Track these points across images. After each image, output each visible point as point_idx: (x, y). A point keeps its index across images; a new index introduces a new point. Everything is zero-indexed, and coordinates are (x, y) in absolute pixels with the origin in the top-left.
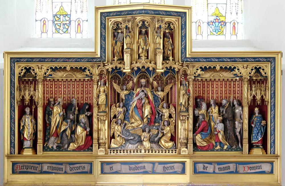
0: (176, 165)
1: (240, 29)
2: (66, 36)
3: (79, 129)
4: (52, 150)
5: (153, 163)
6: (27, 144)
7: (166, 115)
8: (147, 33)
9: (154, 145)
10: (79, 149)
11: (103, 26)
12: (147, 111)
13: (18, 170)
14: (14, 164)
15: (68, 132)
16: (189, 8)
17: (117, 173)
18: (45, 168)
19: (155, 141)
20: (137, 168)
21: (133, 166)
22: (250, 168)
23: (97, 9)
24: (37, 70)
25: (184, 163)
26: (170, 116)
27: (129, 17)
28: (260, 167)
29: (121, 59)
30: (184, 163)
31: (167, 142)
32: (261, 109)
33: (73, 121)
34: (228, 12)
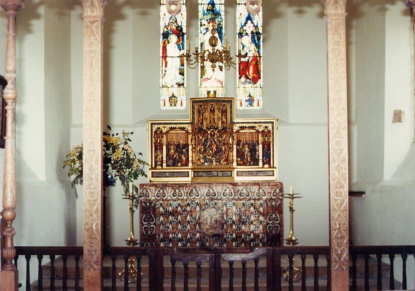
0: (228, 172)
1: (261, 103)
2: (175, 108)
3: (183, 156)
4: (170, 166)
5: (218, 172)
6: (159, 163)
7: (224, 149)
8: (214, 110)
9: (217, 163)
10: (183, 165)
11: (193, 107)
12: (214, 148)
13: (155, 175)
14: (152, 173)
15: (178, 157)
16: (233, 98)
17: (200, 176)
18: (167, 174)
19: (218, 161)
20: (210, 174)
21: (208, 173)
22: (263, 173)
23: (191, 99)
24: (163, 129)
25: (188, 172)
26: (225, 149)
27: (205, 103)
28: (268, 173)
29: (202, 123)
30: (188, 172)
31: (202, 259)
32: (267, 148)
33: (179, 152)
34: (255, 95)
